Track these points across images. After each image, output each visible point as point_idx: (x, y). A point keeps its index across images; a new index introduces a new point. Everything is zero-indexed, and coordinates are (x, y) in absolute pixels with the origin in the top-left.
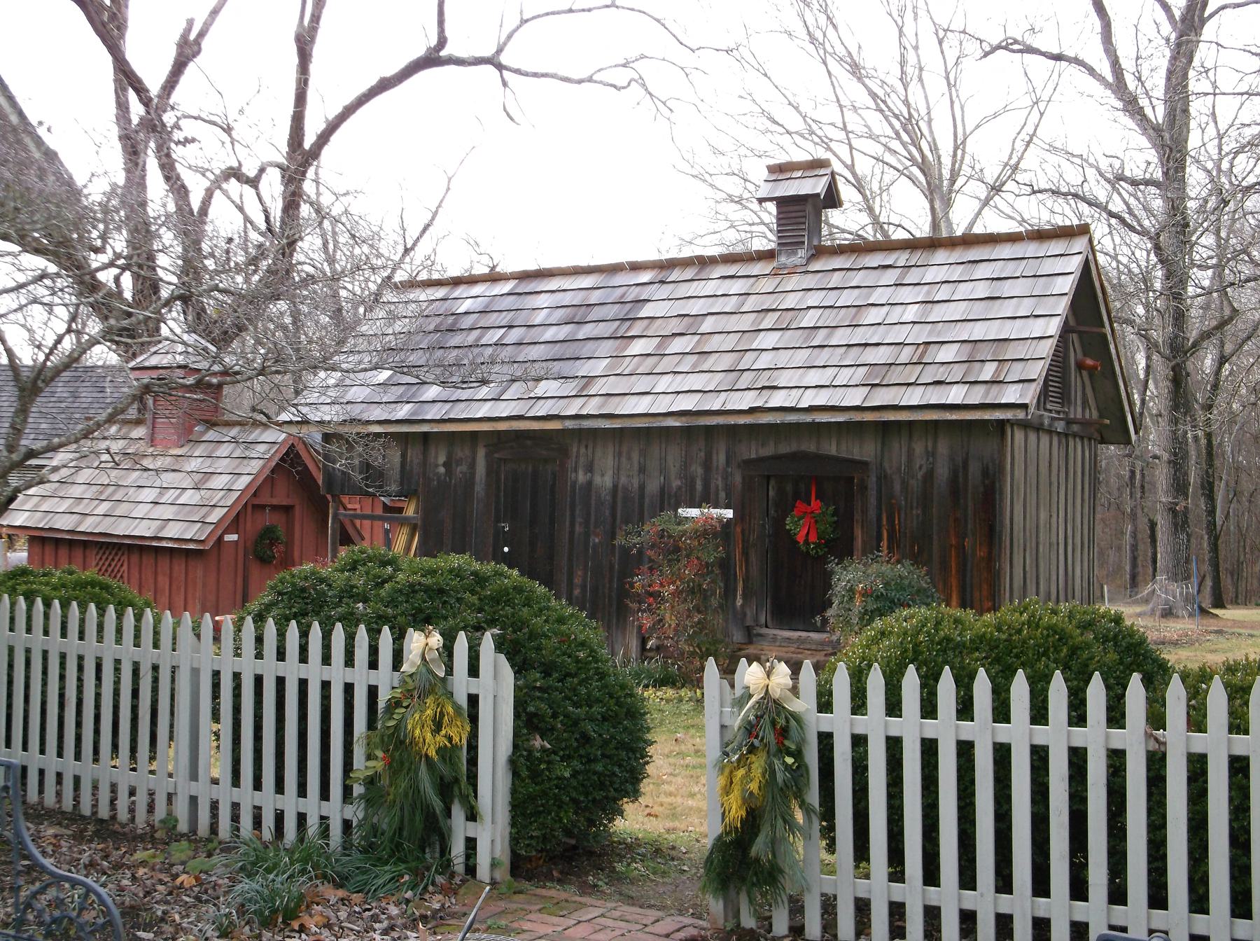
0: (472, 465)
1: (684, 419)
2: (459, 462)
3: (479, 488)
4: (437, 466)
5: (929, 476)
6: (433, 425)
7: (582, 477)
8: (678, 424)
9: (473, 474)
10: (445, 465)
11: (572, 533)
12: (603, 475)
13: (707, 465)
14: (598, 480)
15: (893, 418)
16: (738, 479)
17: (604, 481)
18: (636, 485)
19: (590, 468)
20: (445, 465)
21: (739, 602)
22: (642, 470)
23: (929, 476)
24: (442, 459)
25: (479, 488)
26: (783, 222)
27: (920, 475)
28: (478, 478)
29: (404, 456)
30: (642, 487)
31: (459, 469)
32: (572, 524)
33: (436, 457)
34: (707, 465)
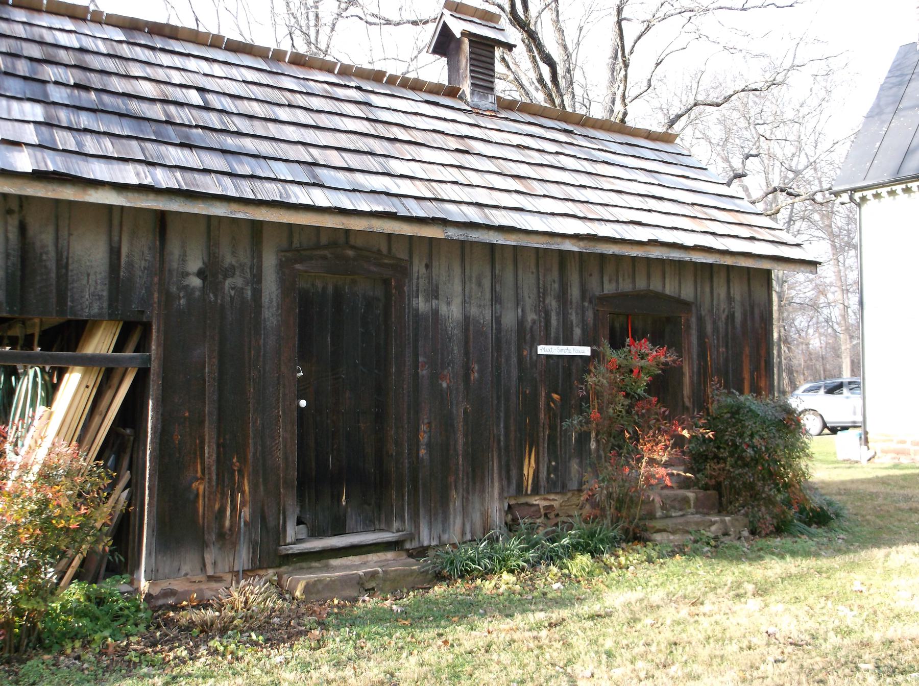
0: (257, 278)
1: (582, 244)
2: (229, 272)
3: (270, 314)
4: (186, 274)
5: (731, 317)
6: (234, 207)
7: (422, 305)
8: (576, 249)
9: (257, 294)
10: (200, 274)
11: (416, 375)
12: (449, 304)
13: (563, 297)
14: (443, 309)
15: (744, 265)
16: (590, 315)
17: (452, 311)
18: (488, 317)
19: (434, 293)
20: (200, 274)
21: (593, 445)
22: (496, 299)
23: (731, 317)
24: (194, 264)
25: (270, 314)
26: (473, 56)
27: (723, 317)
28: (265, 300)
29: (114, 253)
30: (498, 320)
31: (228, 282)
32: (416, 366)
33: (183, 259)
34: (563, 297)
